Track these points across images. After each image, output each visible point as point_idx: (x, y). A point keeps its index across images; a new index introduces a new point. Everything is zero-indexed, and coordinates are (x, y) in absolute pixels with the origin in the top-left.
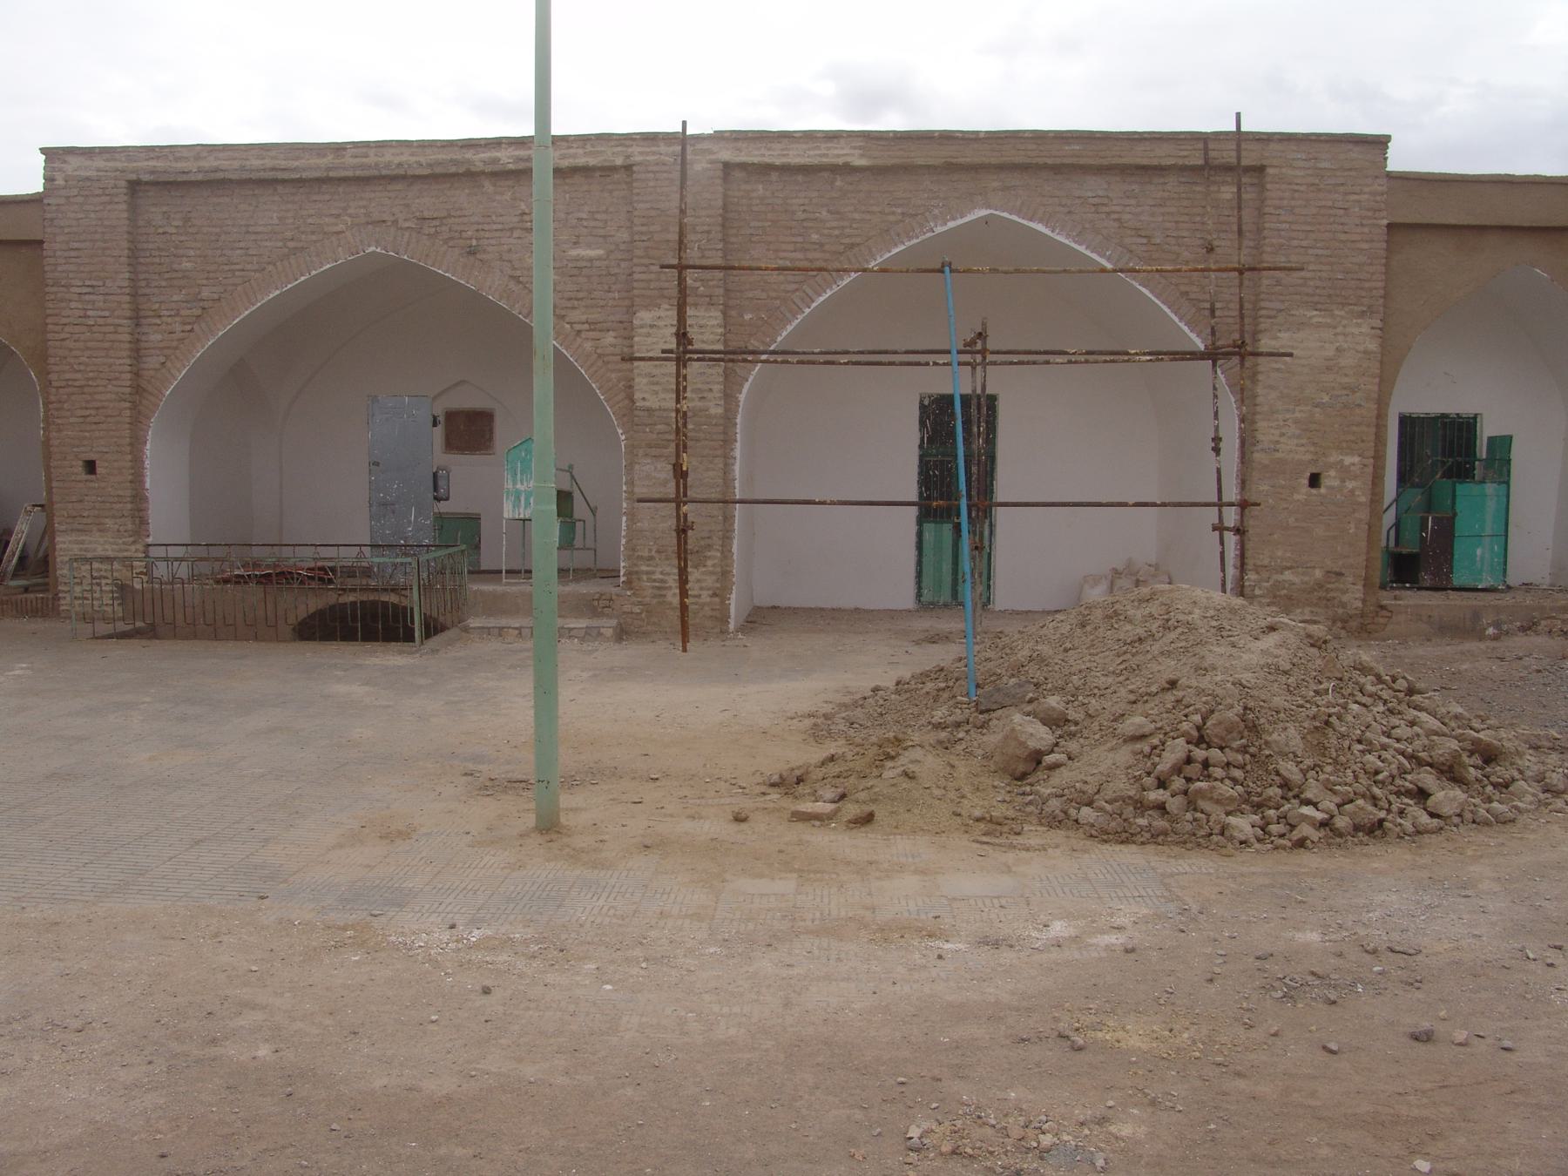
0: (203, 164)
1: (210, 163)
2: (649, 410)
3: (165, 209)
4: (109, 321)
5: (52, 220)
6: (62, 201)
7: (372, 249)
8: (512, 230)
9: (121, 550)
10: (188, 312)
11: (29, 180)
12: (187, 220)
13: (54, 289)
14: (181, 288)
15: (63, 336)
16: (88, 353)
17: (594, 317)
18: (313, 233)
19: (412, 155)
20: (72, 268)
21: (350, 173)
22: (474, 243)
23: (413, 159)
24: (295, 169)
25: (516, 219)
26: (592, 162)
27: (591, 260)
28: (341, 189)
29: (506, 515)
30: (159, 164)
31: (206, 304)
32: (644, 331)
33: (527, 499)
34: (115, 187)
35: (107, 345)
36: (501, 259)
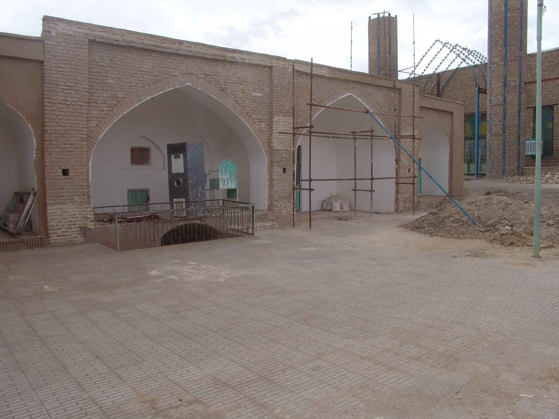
0: (125, 38)
1: (128, 38)
2: (277, 150)
3: (101, 54)
4: (78, 103)
5: (49, 51)
6: (55, 43)
7: (188, 84)
8: (235, 83)
9: (83, 211)
10: (111, 102)
11: (35, 30)
12: (111, 61)
13: (49, 85)
14: (107, 91)
15: (53, 109)
16: (67, 118)
17: (259, 117)
18: (166, 74)
19: (207, 50)
20: (60, 76)
21: (185, 53)
22: (223, 86)
23: (207, 52)
24: (164, 48)
25: (236, 80)
26: (262, 63)
27: (258, 97)
28: (177, 58)
29: (220, 188)
30: (106, 35)
31: (119, 99)
32: (276, 123)
33: (227, 181)
34: (83, 41)
35: (76, 114)
36: (232, 94)
